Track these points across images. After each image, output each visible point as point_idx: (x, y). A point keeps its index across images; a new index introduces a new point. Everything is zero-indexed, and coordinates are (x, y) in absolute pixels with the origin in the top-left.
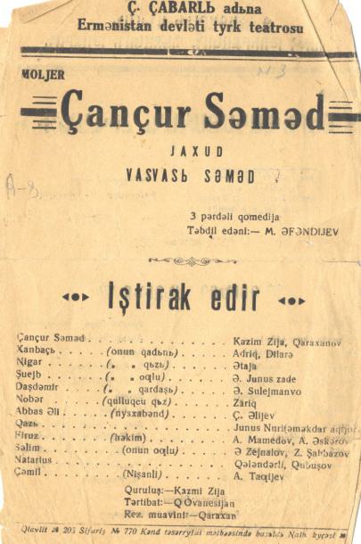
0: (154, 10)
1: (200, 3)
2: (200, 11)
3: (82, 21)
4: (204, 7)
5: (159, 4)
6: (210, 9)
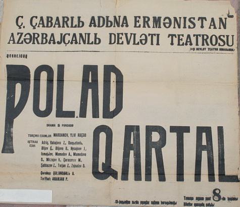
0: (34, 24)
1: (72, 18)
2: (72, 27)
3: (181, 37)
4: (76, 22)
5: (39, 18)
6: (81, 24)
